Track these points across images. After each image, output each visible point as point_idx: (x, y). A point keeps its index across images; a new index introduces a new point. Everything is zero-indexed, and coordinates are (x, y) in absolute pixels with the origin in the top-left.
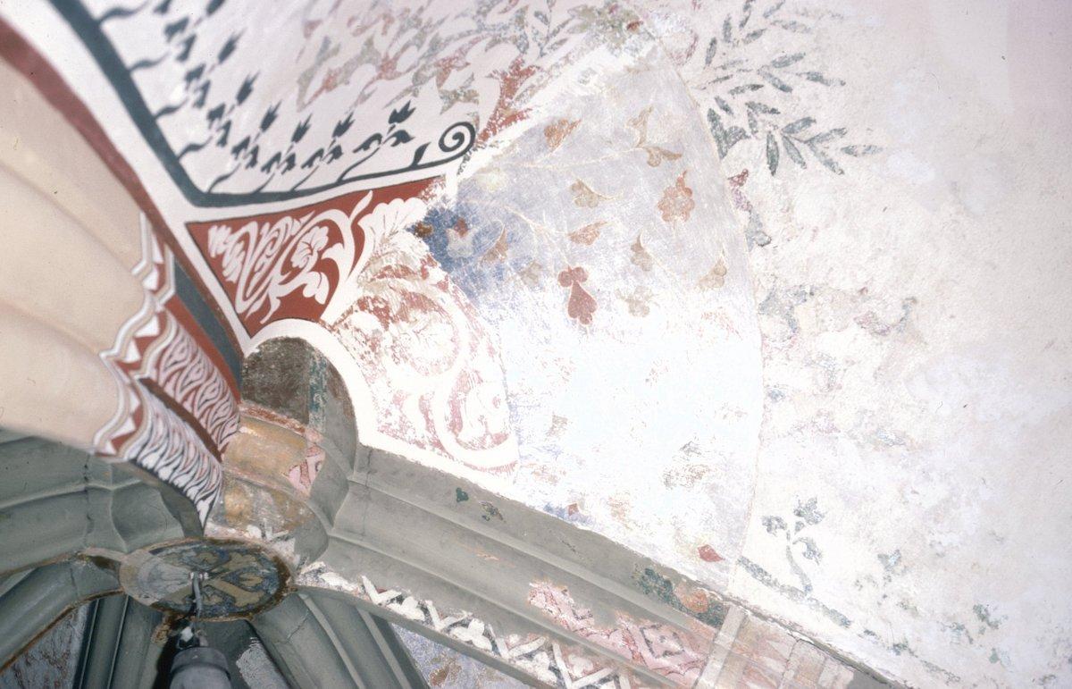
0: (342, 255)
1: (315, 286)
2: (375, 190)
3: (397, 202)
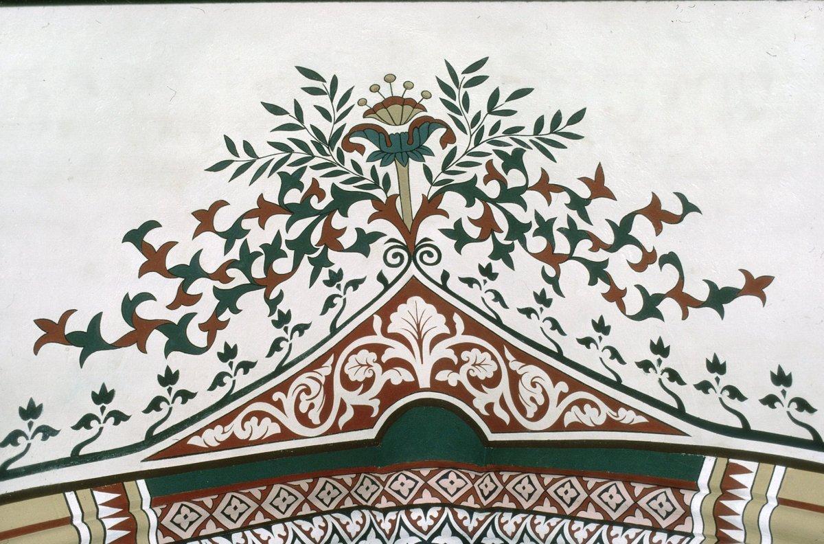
0: (397, 350)
1: (398, 376)
2: (377, 313)
3: (401, 307)
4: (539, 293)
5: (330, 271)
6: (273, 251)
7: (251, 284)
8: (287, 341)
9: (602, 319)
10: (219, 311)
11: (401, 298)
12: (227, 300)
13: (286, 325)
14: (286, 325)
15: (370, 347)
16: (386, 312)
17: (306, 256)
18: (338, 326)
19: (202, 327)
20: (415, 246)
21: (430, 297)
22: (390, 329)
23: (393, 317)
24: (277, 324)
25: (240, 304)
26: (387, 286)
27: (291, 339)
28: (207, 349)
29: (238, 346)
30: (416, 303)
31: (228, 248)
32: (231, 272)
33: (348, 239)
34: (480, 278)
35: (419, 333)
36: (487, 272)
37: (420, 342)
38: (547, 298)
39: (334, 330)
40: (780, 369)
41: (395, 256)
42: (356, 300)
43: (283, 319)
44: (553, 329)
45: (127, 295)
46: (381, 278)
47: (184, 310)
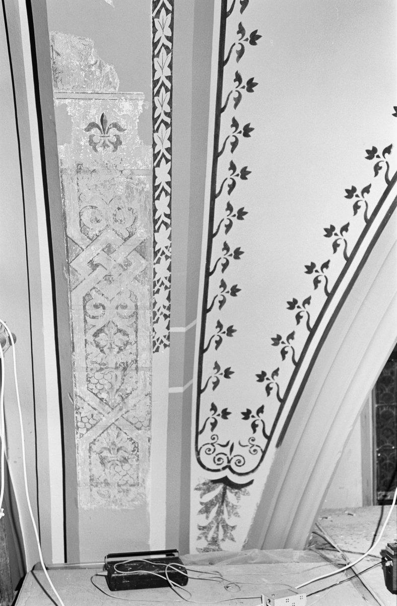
4: (257, 34)
9: (246, 213)
29: (254, 131)
34: (244, 83)
38: (253, 88)
40: (250, 172)
45: (243, 208)
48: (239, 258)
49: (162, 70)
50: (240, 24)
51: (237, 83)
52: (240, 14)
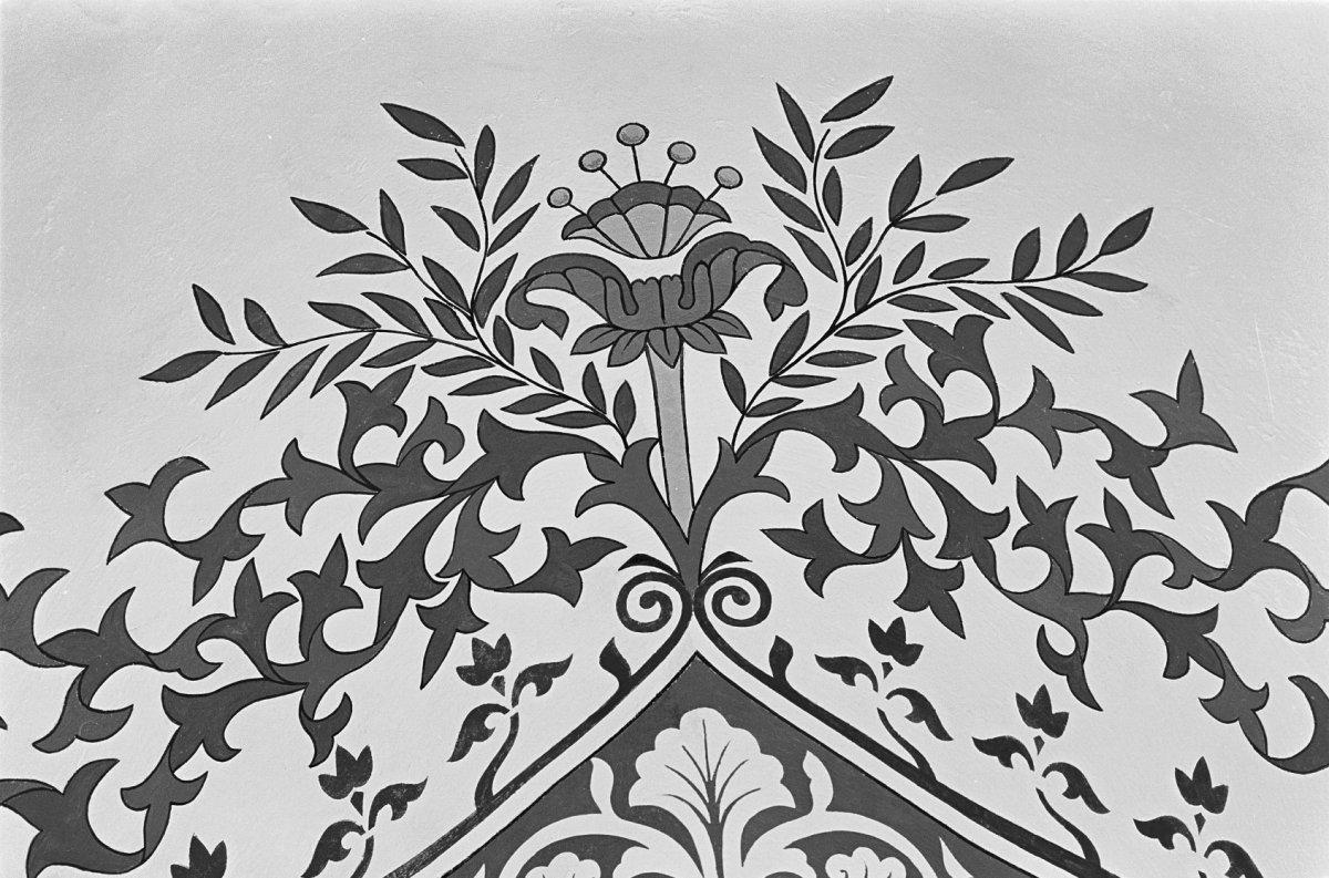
3: (665, 738)
5: (476, 642)
6: (323, 591)
7: (266, 678)
8: (360, 830)
9: (1202, 767)
10: (176, 753)
11: (664, 712)
12: (201, 724)
13: (359, 789)
14: (359, 789)
15: (582, 846)
16: (625, 750)
17: (412, 603)
18: (496, 788)
19: (130, 797)
20: (701, 576)
21: (741, 711)
22: (637, 797)
23: (643, 762)
24: (333, 787)
25: (235, 732)
26: (628, 682)
27: (371, 825)
28: (142, 857)
30: (704, 724)
31: (203, 585)
32: (210, 649)
33: (524, 559)
35: (713, 807)
36: (892, 642)
37: (715, 831)
38: (1214, 784)
39: (487, 800)
41: (647, 601)
42: (544, 719)
43: (354, 770)
44: (1070, 794)
46: (611, 659)
47: (81, 753)
48: (1223, 790)
49: (1101, 254)
50: (1143, 827)
51: (860, 678)
52: (1008, 769)
